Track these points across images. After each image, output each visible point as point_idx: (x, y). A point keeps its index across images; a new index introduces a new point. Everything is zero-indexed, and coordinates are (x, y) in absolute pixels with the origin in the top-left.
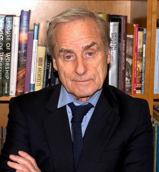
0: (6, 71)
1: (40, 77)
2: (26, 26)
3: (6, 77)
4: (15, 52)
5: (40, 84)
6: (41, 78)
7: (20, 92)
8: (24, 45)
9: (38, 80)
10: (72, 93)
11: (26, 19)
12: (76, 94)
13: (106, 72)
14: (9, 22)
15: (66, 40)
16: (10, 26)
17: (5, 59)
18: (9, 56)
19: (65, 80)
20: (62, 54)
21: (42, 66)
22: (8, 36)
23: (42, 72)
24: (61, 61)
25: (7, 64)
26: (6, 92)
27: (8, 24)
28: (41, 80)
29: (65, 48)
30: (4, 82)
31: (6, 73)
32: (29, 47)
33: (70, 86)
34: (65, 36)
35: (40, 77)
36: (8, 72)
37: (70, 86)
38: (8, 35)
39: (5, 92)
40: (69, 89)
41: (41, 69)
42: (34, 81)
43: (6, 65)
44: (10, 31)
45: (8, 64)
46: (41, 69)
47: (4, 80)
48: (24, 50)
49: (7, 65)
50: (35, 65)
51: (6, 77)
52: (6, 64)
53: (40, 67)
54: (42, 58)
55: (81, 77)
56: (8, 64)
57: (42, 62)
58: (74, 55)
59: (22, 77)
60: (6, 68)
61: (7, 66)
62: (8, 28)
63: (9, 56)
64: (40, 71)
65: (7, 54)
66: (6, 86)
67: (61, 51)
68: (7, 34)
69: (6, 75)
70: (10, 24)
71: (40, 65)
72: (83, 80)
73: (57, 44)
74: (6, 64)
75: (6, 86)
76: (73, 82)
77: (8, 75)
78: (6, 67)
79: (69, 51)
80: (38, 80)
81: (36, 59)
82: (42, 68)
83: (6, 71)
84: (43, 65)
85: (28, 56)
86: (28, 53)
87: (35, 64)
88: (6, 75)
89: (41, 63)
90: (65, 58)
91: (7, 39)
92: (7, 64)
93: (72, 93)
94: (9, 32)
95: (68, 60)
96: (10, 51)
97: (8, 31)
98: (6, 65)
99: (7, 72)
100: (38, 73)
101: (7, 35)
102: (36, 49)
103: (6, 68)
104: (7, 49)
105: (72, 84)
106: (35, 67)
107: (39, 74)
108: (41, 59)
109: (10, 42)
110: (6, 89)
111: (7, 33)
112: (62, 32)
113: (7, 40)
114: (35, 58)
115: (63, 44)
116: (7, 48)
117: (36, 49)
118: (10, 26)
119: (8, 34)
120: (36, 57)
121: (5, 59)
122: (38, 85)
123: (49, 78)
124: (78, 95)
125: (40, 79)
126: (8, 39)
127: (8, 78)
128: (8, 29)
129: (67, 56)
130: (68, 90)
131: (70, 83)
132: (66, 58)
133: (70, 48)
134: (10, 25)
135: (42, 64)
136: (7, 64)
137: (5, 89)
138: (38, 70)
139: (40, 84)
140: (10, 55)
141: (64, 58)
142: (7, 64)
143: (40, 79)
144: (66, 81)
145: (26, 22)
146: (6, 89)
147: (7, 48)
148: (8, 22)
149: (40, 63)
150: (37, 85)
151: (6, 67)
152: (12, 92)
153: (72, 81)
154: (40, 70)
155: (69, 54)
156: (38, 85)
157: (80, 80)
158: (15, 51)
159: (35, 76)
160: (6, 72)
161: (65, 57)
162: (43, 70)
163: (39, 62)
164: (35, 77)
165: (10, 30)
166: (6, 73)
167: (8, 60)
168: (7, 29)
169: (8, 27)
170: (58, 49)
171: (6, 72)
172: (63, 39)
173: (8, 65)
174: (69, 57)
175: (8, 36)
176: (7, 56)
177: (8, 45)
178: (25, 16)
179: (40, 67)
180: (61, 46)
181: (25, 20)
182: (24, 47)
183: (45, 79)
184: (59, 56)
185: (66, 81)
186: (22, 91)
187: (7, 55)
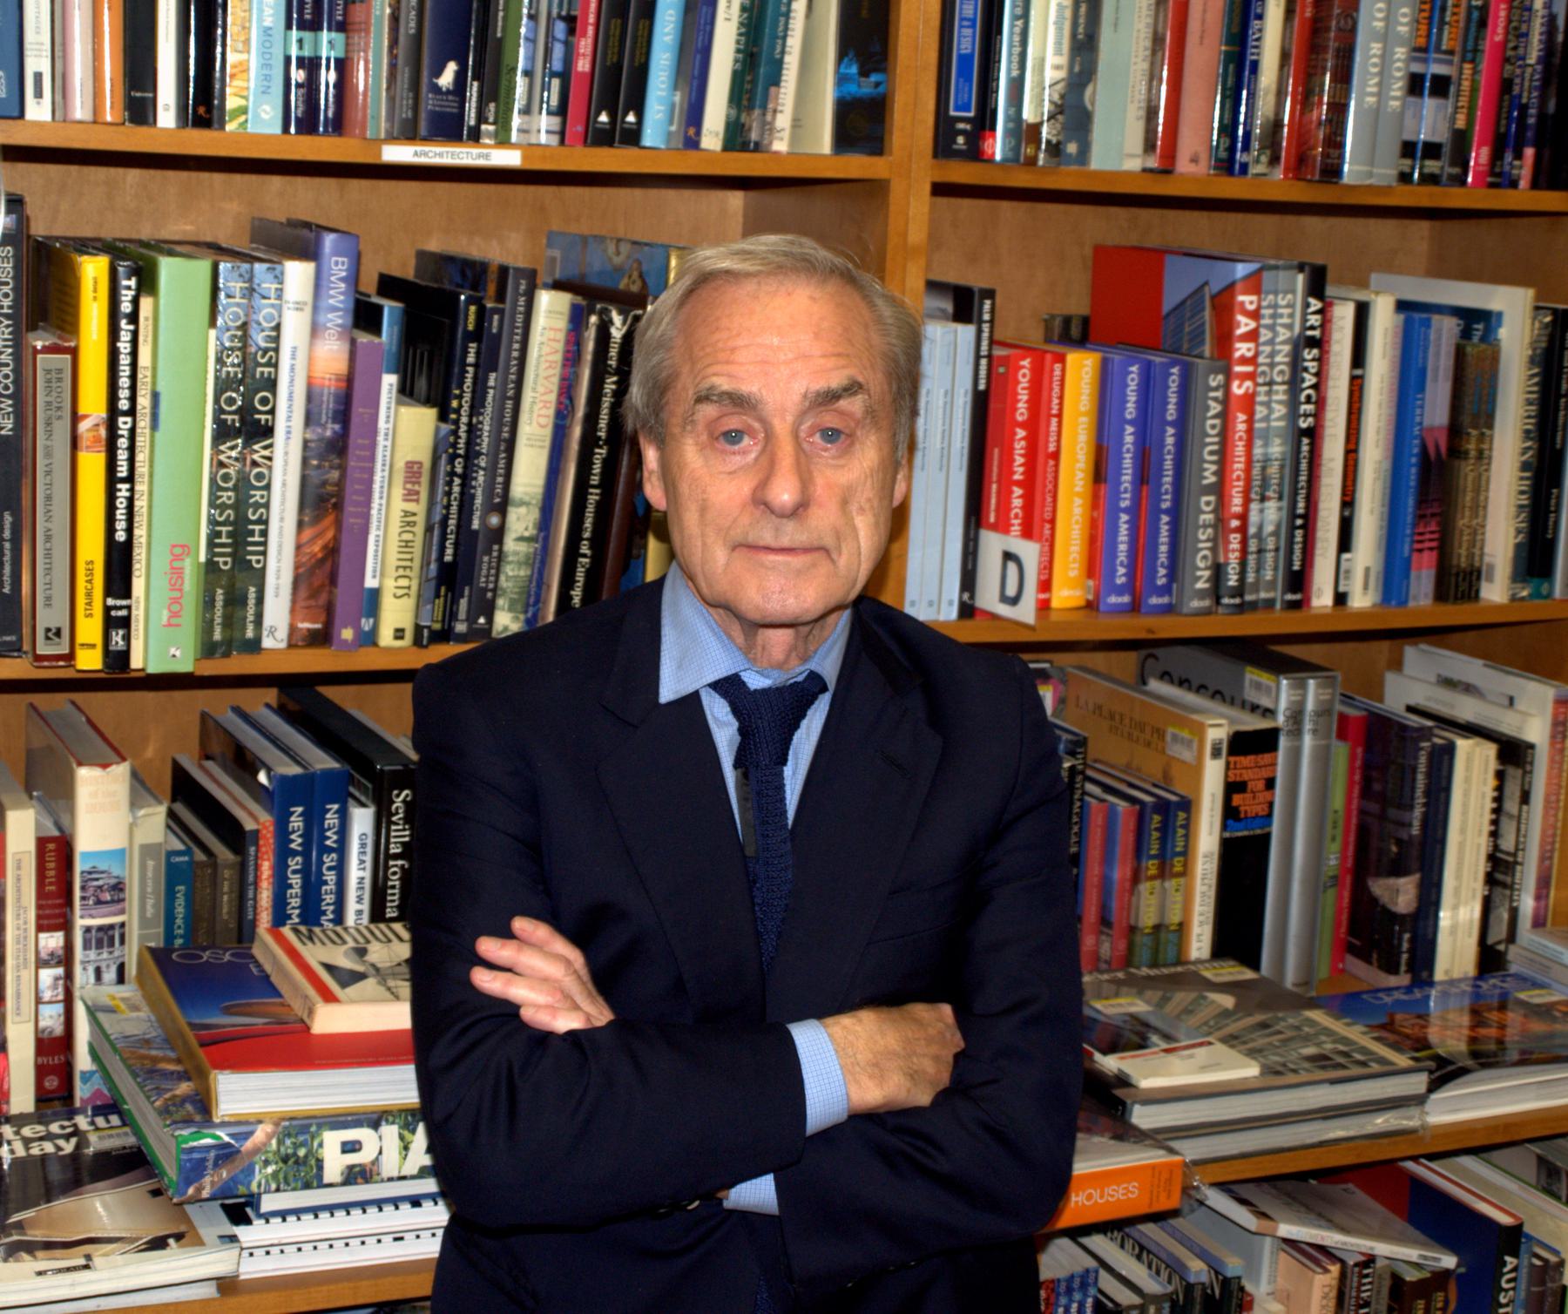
0: (251, 527)
1: (408, 556)
2: (341, 306)
3: (249, 557)
4: (289, 432)
5: (406, 591)
6: (411, 560)
7: (309, 630)
8: (332, 399)
9: (401, 572)
10: (723, 607)
11: (344, 274)
12: (743, 608)
13: (681, 531)
14: (270, 289)
15: (733, 350)
16: (238, 305)
17: (248, 469)
18: (266, 453)
19: (699, 544)
20: (708, 411)
21: (417, 501)
22: (263, 357)
23: (419, 530)
24: (691, 454)
25: (259, 493)
26: (250, 634)
27: (264, 297)
28: (411, 568)
29: (724, 384)
30: (238, 585)
31: (250, 539)
32: (361, 410)
33: (720, 571)
34: (734, 332)
35: (408, 556)
36: (228, 537)
37: (720, 571)
38: (266, 351)
39: (244, 634)
40: (710, 586)
41: (414, 514)
42: (378, 574)
43: (252, 501)
44: (239, 333)
45: (230, 494)
46: (414, 514)
47: (240, 576)
48: (334, 422)
49: (224, 499)
50: (381, 498)
51: (249, 557)
52: (252, 492)
53: (411, 507)
54: (420, 463)
55: (777, 529)
56: (262, 497)
57: (419, 483)
58: (756, 425)
59: (320, 555)
60: (254, 514)
61: (257, 506)
62: (264, 318)
63: (266, 453)
64: (408, 528)
65: (256, 447)
66: (252, 602)
67: (702, 399)
68: (260, 349)
69: (250, 548)
70: (238, 294)
71: (410, 496)
72: (785, 542)
73: (685, 370)
74: (252, 492)
75: (252, 602)
76: (735, 554)
77: (217, 550)
78: (251, 511)
79: (739, 401)
80: (401, 572)
81: (387, 468)
82: (420, 508)
83: (251, 527)
84: (424, 496)
85: (358, 452)
86: (355, 439)
87: (385, 490)
88: (250, 548)
89: (416, 487)
90: (717, 438)
91: (260, 369)
92: (221, 497)
93: (723, 607)
94: (269, 336)
95: (729, 447)
96: (268, 431)
97: (263, 331)
98: (252, 501)
99: (257, 533)
100: (400, 534)
101: (260, 353)
102: (392, 420)
103: (254, 514)
104: (260, 420)
105: (727, 565)
106: (384, 508)
107: (407, 542)
108: (416, 466)
109: (272, 385)
110: (251, 618)
111: (259, 339)
112: (718, 319)
113: (258, 376)
114: (384, 465)
115: (710, 370)
116: (257, 416)
117: (392, 420)
118: (238, 305)
119: (263, 345)
120: (388, 458)
121: (248, 469)
122: (400, 592)
123: (448, 558)
124: (754, 616)
125: (408, 564)
126: (262, 373)
127: (225, 563)
128: (265, 324)
129: (726, 428)
130: (705, 590)
131: (720, 555)
132: (721, 438)
133: (749, 387)
134: (237, 300)
135: (417, 493)
136: (257, 496)
137: (246, 618)
138: (399, 519)
139: (409, 588)
140: (1308, 324)
141: (714, 438)
142: (221, 497)
143: (408, 564)
144: (704, 544)
145: (343, 285)
146: (251, 618)
147: (257, 416)
148: (264, 285)
149: (409, 486)
150: (395, 596)
151: (251, 511)
152: (272, 632)
153: (734, 548)
154: (408, 524)
155: (733, 423)
156: (400, 592)
157: (773, 544)
158: (292, 430)
159: (380, 549)
160: (252, 533)
161: (716, 434)
162: (420, 520)
163: (406, 482)
164: (380, 553)
165: (238, 328)
166: (250, 539)
167: (260, 477)
168: (259, 324)
169: (265, 311)
170: (691, 392)
171: (252, 533)
172: (720, 345)
173: (230, 502)
174: (733, 437)
175: (263, 357)
176: (256, 457)
177: (264, 401)
178: (340, 259)
179: (411, 507)
180: (704, 378)
181: (342, 280)
182: (331, 412)
183: (433, 566)
184: (689, 420)
185: (704, 544)
186: (318, 626)
187: (257, 452)
